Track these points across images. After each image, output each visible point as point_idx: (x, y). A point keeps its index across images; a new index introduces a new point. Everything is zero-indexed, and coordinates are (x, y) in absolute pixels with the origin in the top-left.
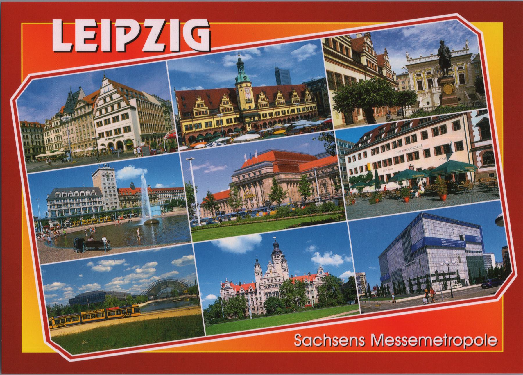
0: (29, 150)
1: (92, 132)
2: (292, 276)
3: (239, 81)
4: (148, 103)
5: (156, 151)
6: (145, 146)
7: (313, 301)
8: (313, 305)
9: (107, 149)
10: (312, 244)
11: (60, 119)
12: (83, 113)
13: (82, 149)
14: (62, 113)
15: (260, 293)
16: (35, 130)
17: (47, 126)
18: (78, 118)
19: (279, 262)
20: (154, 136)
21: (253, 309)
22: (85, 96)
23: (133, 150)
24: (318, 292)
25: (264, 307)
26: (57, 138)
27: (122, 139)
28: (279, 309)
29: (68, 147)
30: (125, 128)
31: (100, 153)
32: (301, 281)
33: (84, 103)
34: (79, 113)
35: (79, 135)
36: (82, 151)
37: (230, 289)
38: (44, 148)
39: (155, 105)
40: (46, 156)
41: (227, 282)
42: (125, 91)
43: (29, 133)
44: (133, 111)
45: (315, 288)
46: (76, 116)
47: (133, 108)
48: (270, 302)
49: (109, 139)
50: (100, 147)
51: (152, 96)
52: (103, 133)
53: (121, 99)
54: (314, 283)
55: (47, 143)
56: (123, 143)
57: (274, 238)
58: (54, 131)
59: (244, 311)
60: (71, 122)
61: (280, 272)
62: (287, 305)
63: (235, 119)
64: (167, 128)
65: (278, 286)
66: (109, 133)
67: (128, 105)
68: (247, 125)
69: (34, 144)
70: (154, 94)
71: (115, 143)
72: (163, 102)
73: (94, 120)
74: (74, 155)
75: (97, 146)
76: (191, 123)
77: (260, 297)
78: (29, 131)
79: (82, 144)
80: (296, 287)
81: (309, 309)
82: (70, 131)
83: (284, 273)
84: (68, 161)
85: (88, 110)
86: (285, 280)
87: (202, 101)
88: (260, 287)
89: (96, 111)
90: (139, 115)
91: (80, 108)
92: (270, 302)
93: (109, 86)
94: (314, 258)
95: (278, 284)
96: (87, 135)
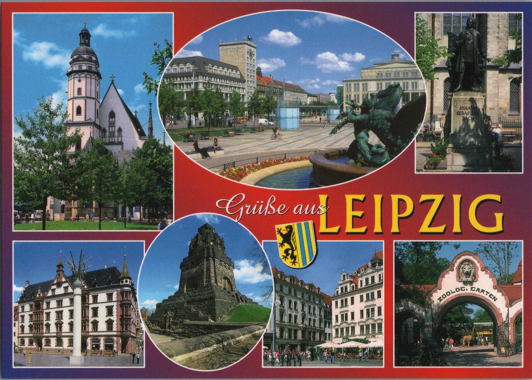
0: (296, 332)
16: (309, 297)
69: (306, 322)
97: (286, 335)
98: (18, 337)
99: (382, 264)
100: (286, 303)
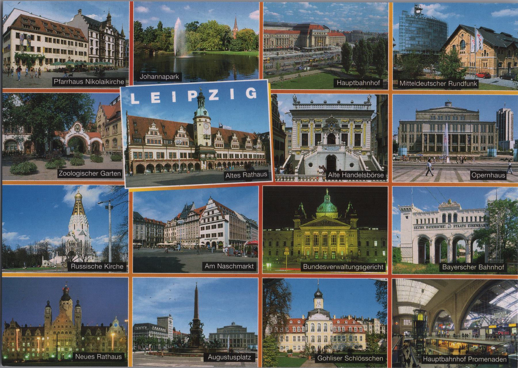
0: (153, 239)
3: (198, 115)
18: (189, 222)
20: (238, 242)
27: (216, 241)
33: (194, 213)
46: (188, 221)
47: (226, 221)
50: (201, 244)
63: (189, 154)
66: (208, 236)
68: (202, 162)
69: (157, 235)
71: (211, 243)
76: (141, 150)
78: (155, 227)
85: (196, 218)
87: (157, 128)
91: (191, 216)
97: (149, 240)
98: (89, 57)
99: (263, 267)
100: (150, 230)
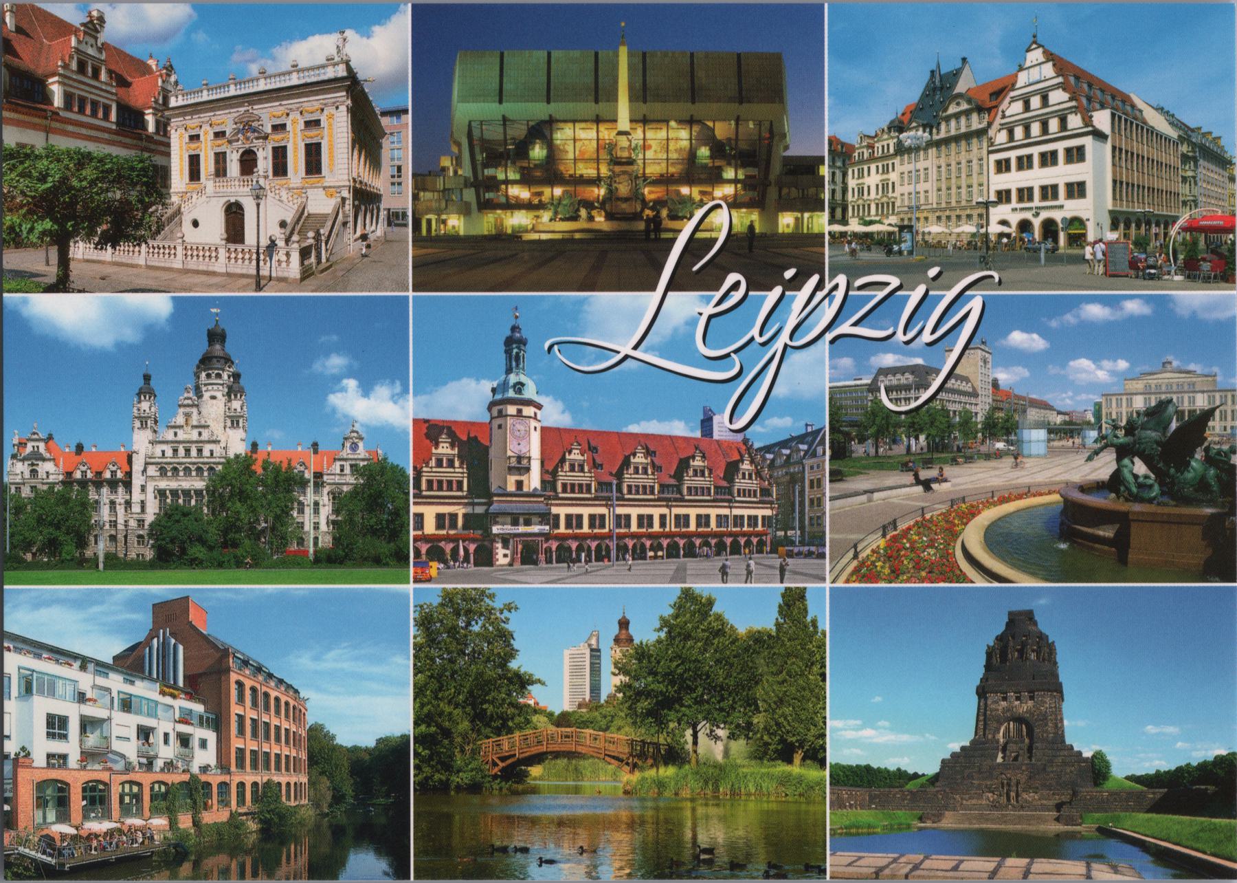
1: (981, 185)
2: (254, 446)
4: (1142, 128)
5: (1146, 260)
6: (1117, 242)
7: (316, 539)
8: (311, 550)
9: (1014, 235)
10: (337, 349)
11: (898, 137)
12: (963, 130)
13: (947, 227)
14: (906, 122)
15: (143, 488)
17: (860, 151)
18: (946, 141)
19: (219, 395)
20: (1146, 220)
21: (113, 538)
22: (973, 85)
23: (1083, 248)
24: (336, 511)
25: (150, 535)
26: (883, 188)
27: (1057, 216)
28: (197, 551)
29: (909, 216)
30: (1069, 186)
31: (991, 245)
32: (285, 466)
33: (969, 101)
34: (953, 128)
35: (944, 187)
36: (947, 231)
37: (44, 460)
38: (845, 210)
39: (1160, 136)
40: (846, 233)
41: (36, 437)
42: (1085, 86)
43: (839, 168)
44: (1099, 144)
45: (326, 498)
46: (943, 135)
47: (1099, 135)
48: (169, 524)
49: (1022, 209)
50: (994, 229)
51: (1156, 109)
52: (1008, 192)
53: (1071, 108)
54: (325, 478)
55: (853, 196)
56: (1061, 226)
57: (214, 310)
58: (877, 167)
59: (82, 543)
60: (926, 149)
61: (217, 428)
62: (226, 540)
64: (1185, 203)
65: (206, 474)
66: (1025, 194)
67: (1086, 125)
70: (1162, 105)
71: (1037, 223)
72: (1183, 130)
73: (990, 152)
74: (923, 239)
75: (988, 224)
77: (142, 502)
79: (948, 213)
80: (265, 486)
81: (299, 565)
82: (922, 173)
83: (230, 432)
84: (905, 253)
85: (976, 123)
86: (232, 456)
88: (145, 471)
89: (999, 131)
90: (1114, 157)
91: (957, 116)
92: (169, 524)
93: (1043, 66)
94: (339, 395)
95: (205, 467)
96: (964, 191)
